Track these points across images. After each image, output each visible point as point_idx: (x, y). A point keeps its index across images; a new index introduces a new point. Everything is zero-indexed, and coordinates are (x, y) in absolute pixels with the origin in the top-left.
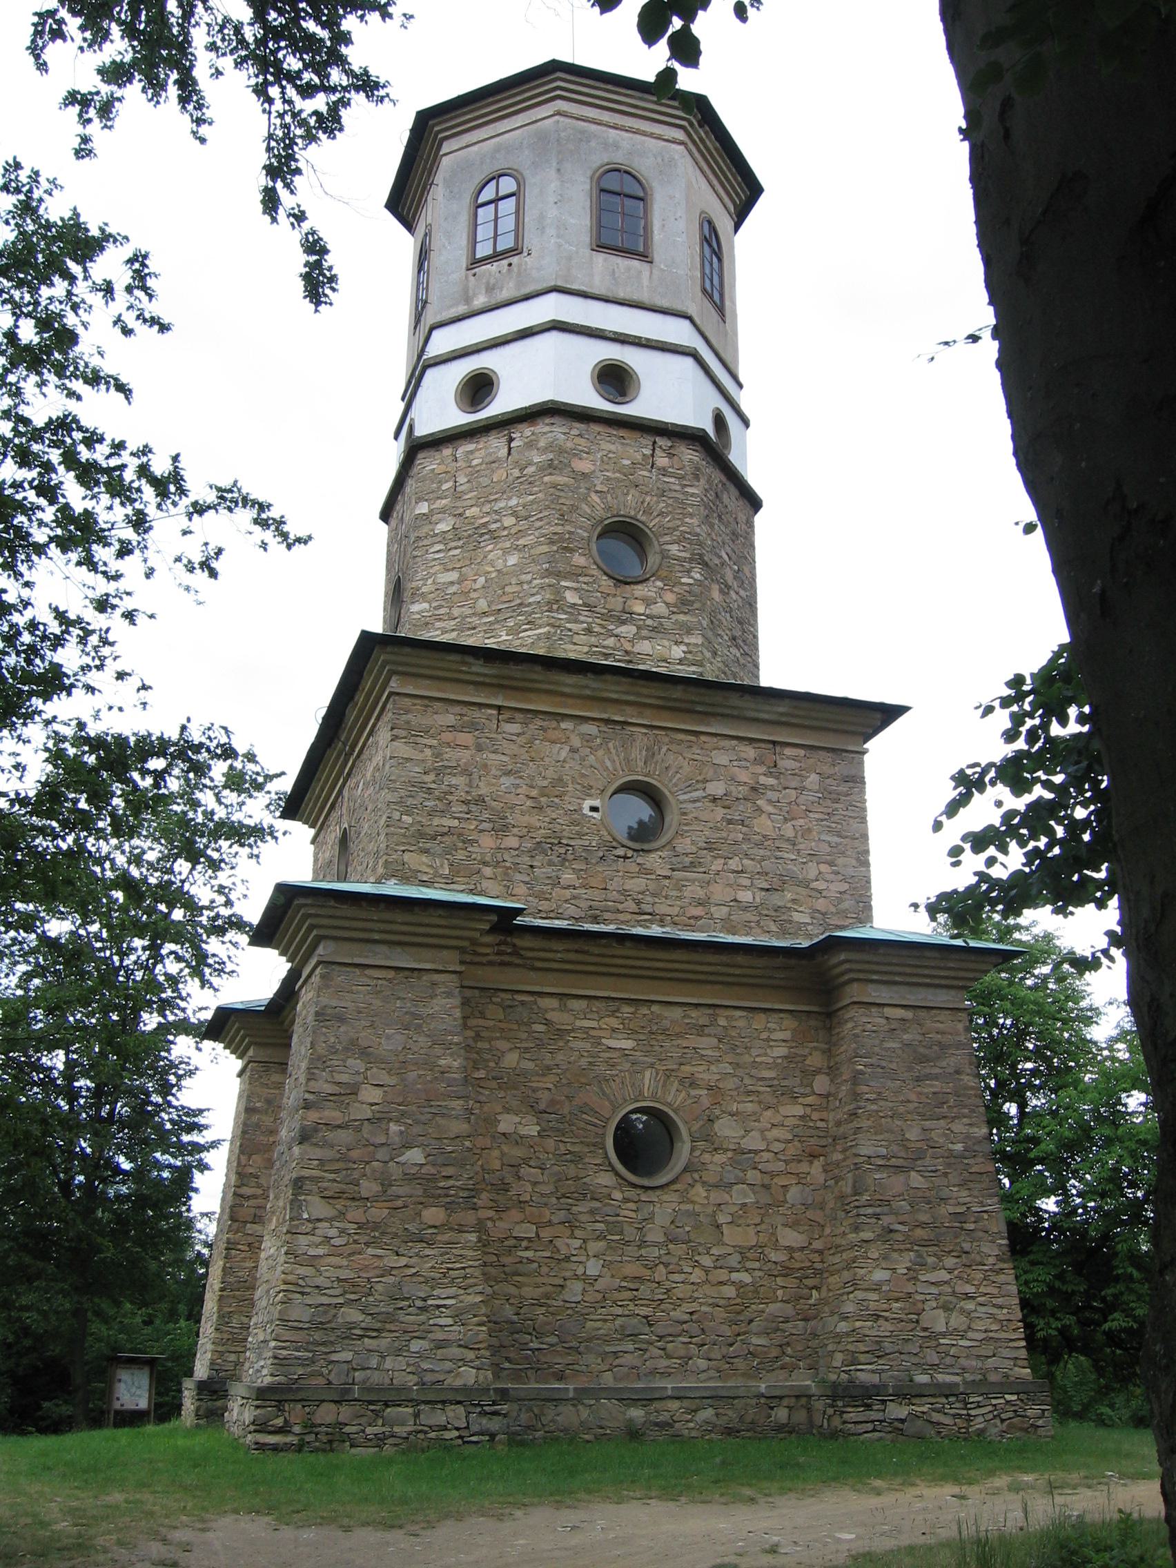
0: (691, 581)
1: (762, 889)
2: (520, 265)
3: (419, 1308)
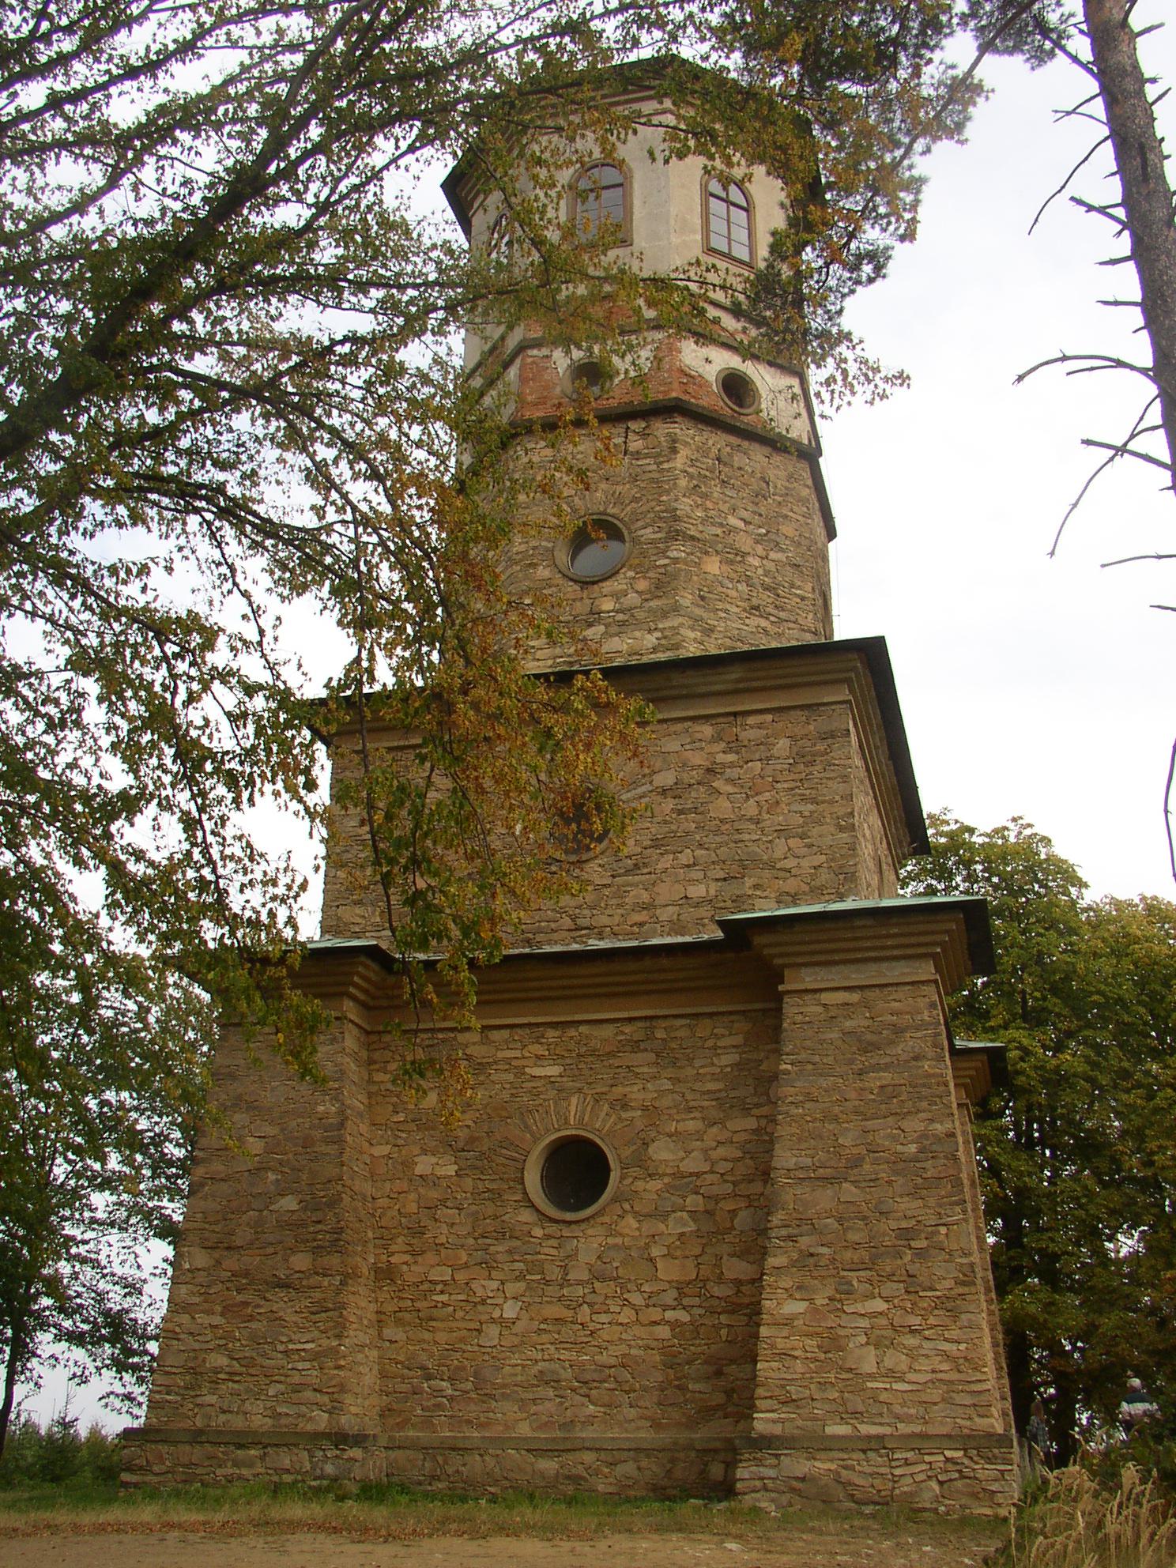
0: (666, 561)
1: (717, 880)
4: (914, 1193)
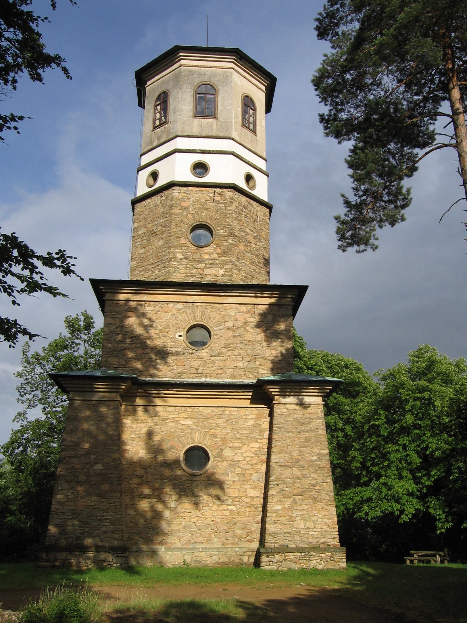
0: (228, 244)
2: (167, 128)
3: (98, 520)
4: (316, 472)
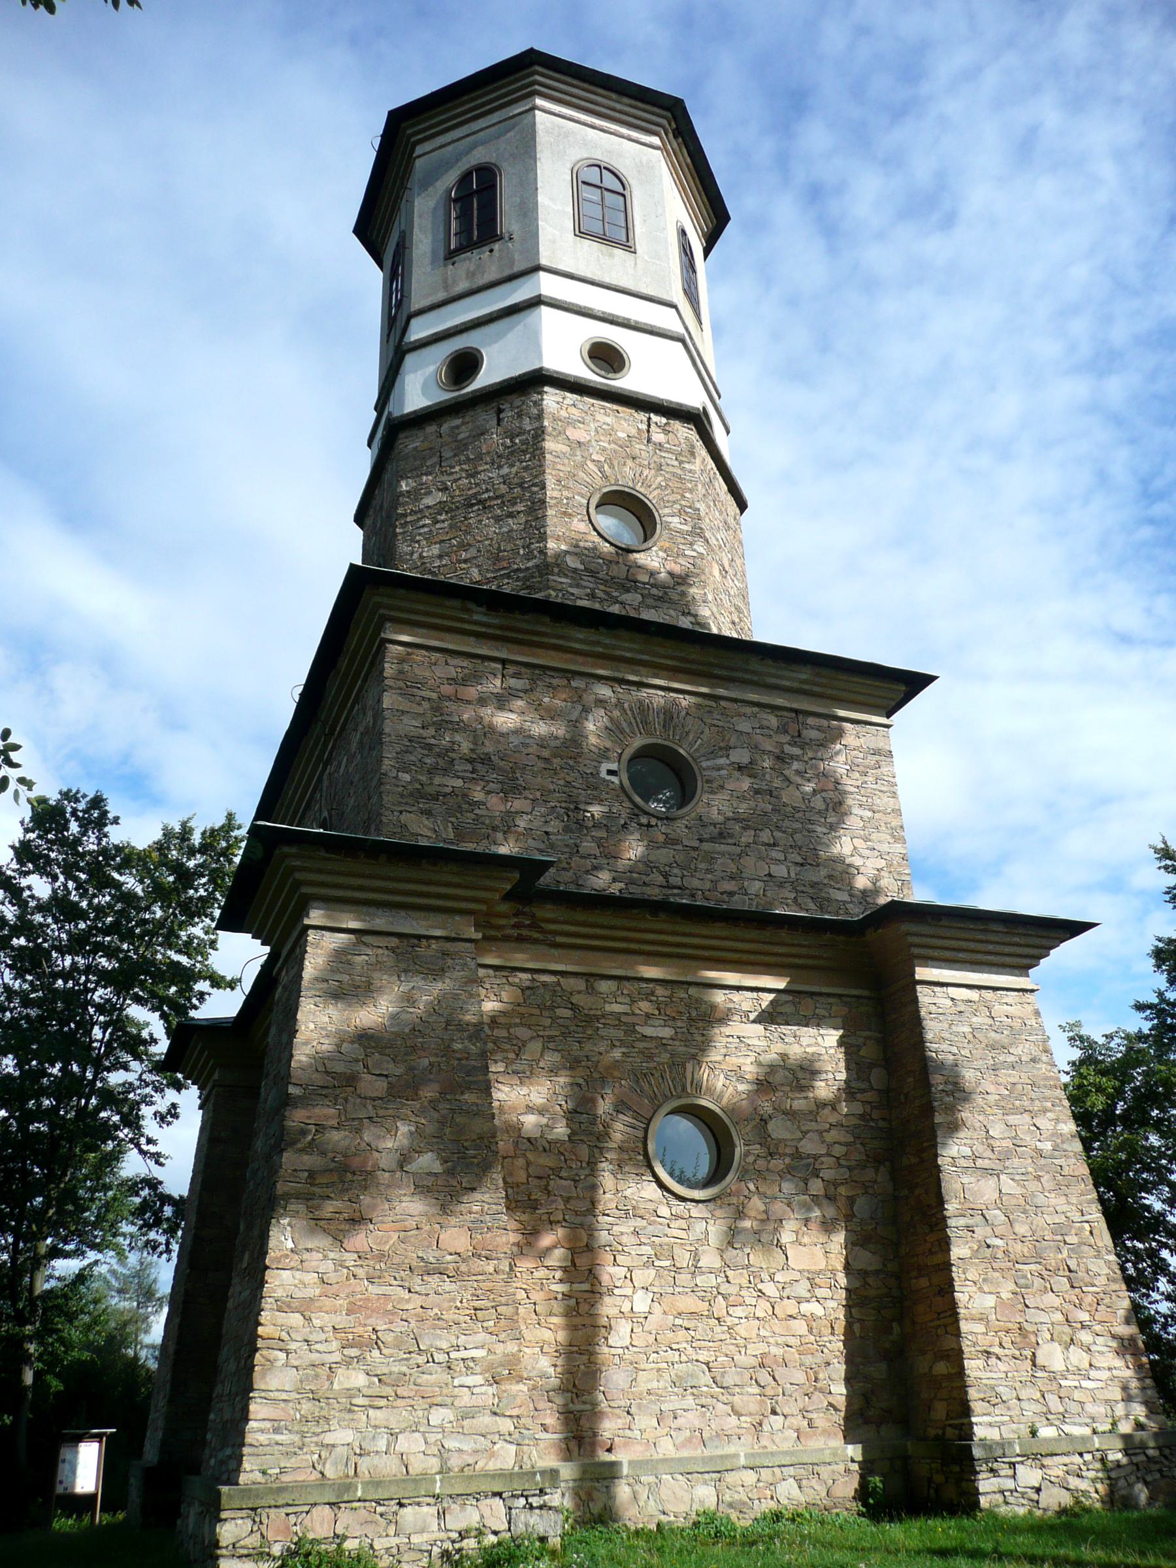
0: (694, 554)
